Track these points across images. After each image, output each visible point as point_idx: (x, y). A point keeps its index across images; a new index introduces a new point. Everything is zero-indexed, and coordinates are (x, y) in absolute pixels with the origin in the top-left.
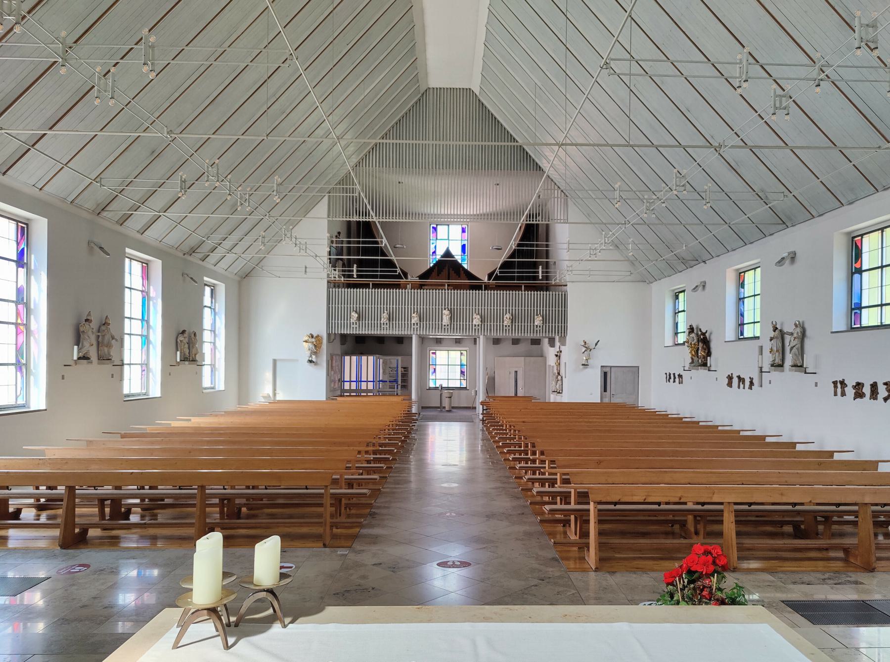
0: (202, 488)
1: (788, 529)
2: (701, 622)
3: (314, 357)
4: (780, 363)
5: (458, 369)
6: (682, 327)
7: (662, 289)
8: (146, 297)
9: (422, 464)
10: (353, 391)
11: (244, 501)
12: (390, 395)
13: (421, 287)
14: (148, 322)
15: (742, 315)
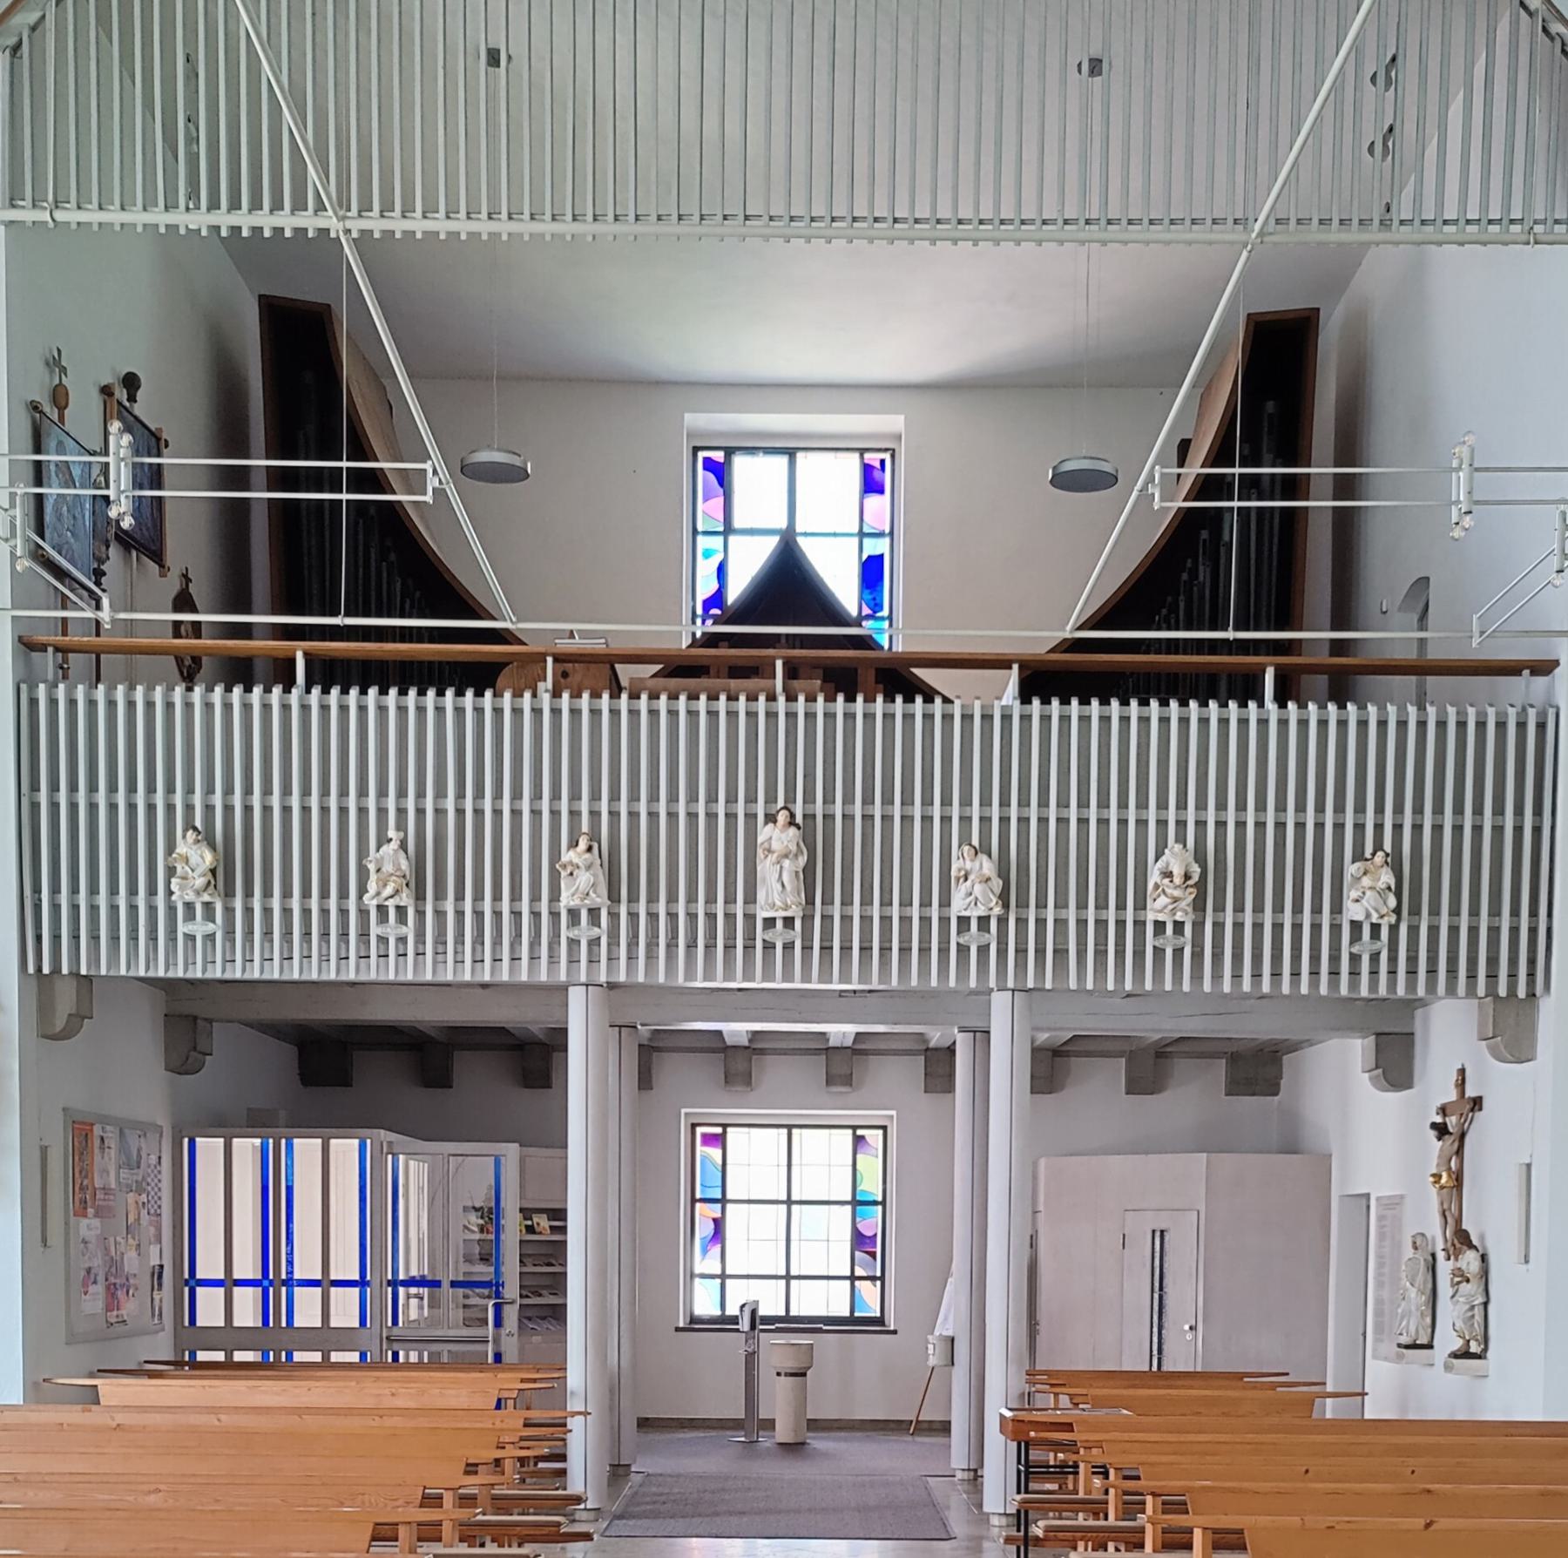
10: (245, 1337)
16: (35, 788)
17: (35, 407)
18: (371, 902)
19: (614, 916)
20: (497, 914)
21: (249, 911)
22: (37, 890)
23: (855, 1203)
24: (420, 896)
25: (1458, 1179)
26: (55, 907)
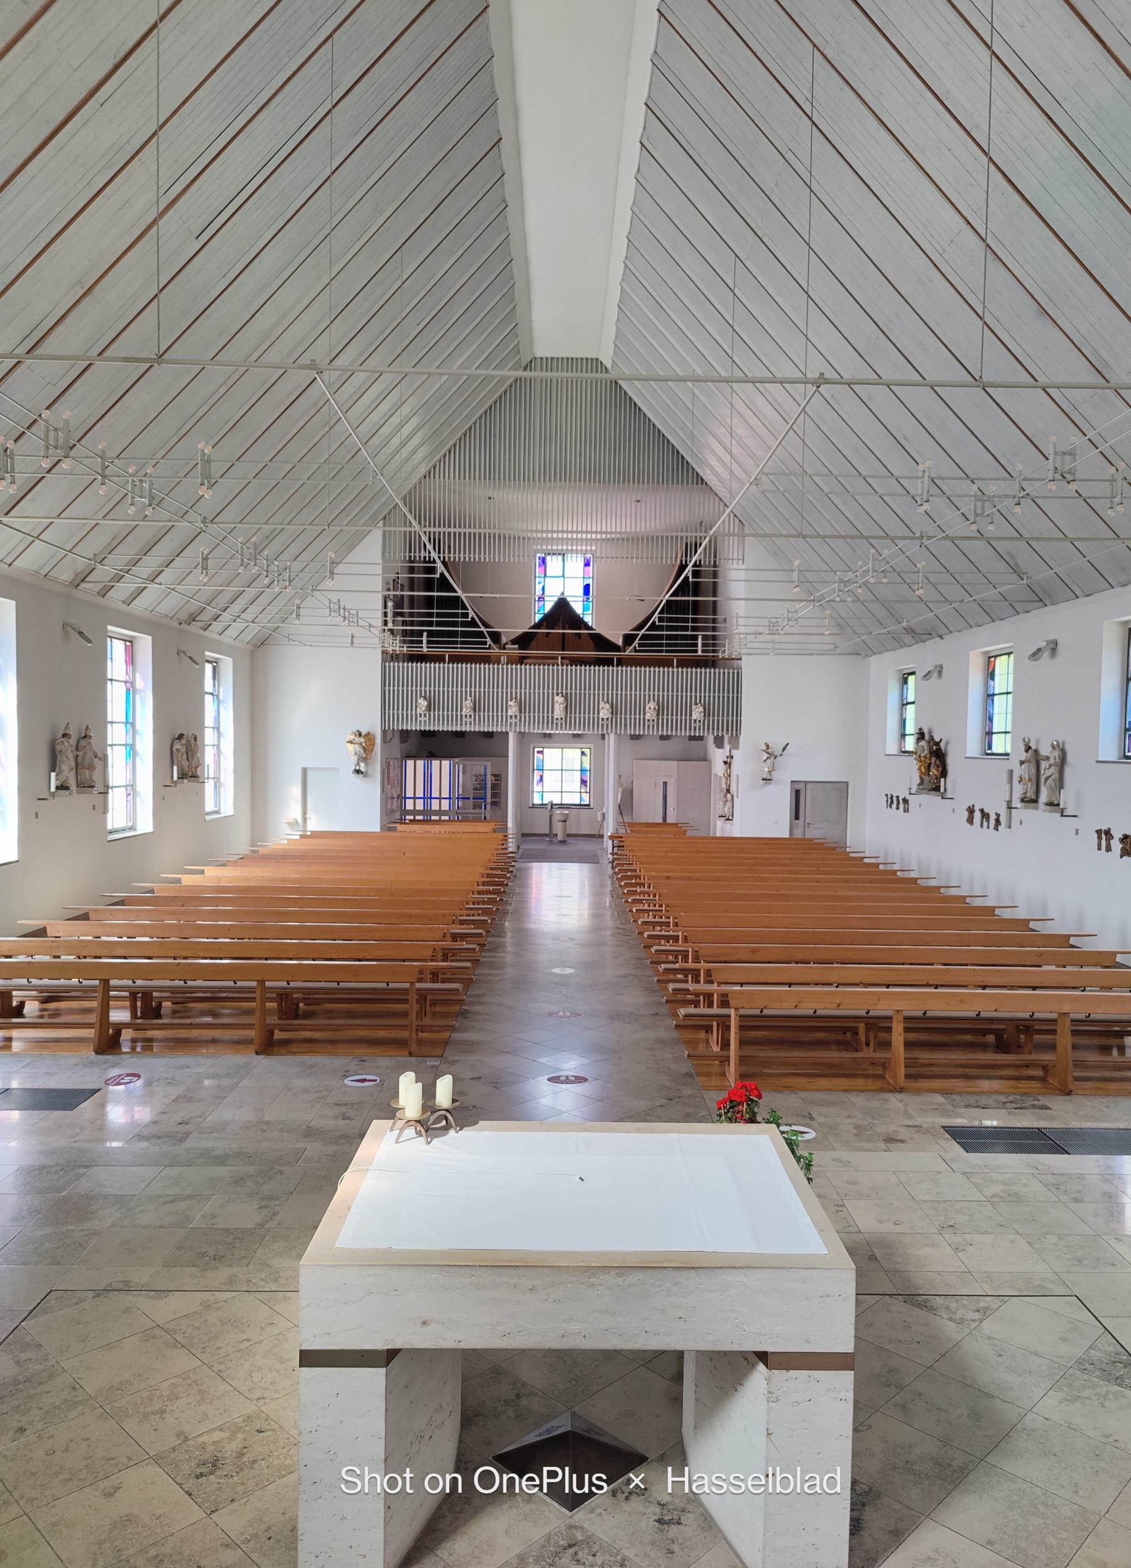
0: (262, 982)
1: (991, 1038)
3: (362, 765)
4: (1034, 797)
5: (577, 776)
6: (911, 728)
7: (884, 668)
8: (131, 689)
9: (524, 937)
10: (419, 812)
11: (301, 996)
13: (521, 660)
14: (133, 725)
15: (991, 720)
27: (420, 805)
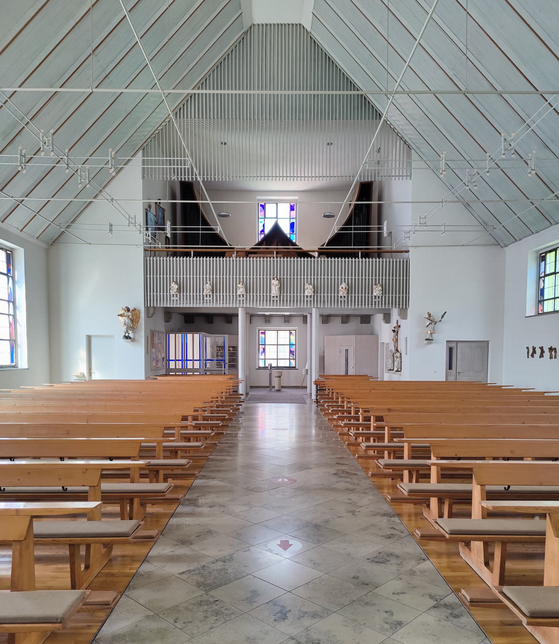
2: (513, 585)
3: (130, 332)
10: (179, 370)
12: (217, 374)
16: (147, 275)
17: (146, 209)
18: (205, 294)
19: (247, 296)
20: (226, 296)
21: (183, 295)
22: (147, 292)
23: (290, 345)
24: (213, 293)
25: (397, 340)
26: (150, 295)
27: (179, 365)
